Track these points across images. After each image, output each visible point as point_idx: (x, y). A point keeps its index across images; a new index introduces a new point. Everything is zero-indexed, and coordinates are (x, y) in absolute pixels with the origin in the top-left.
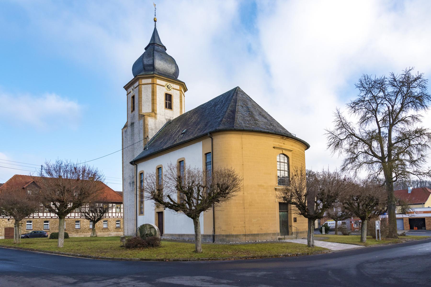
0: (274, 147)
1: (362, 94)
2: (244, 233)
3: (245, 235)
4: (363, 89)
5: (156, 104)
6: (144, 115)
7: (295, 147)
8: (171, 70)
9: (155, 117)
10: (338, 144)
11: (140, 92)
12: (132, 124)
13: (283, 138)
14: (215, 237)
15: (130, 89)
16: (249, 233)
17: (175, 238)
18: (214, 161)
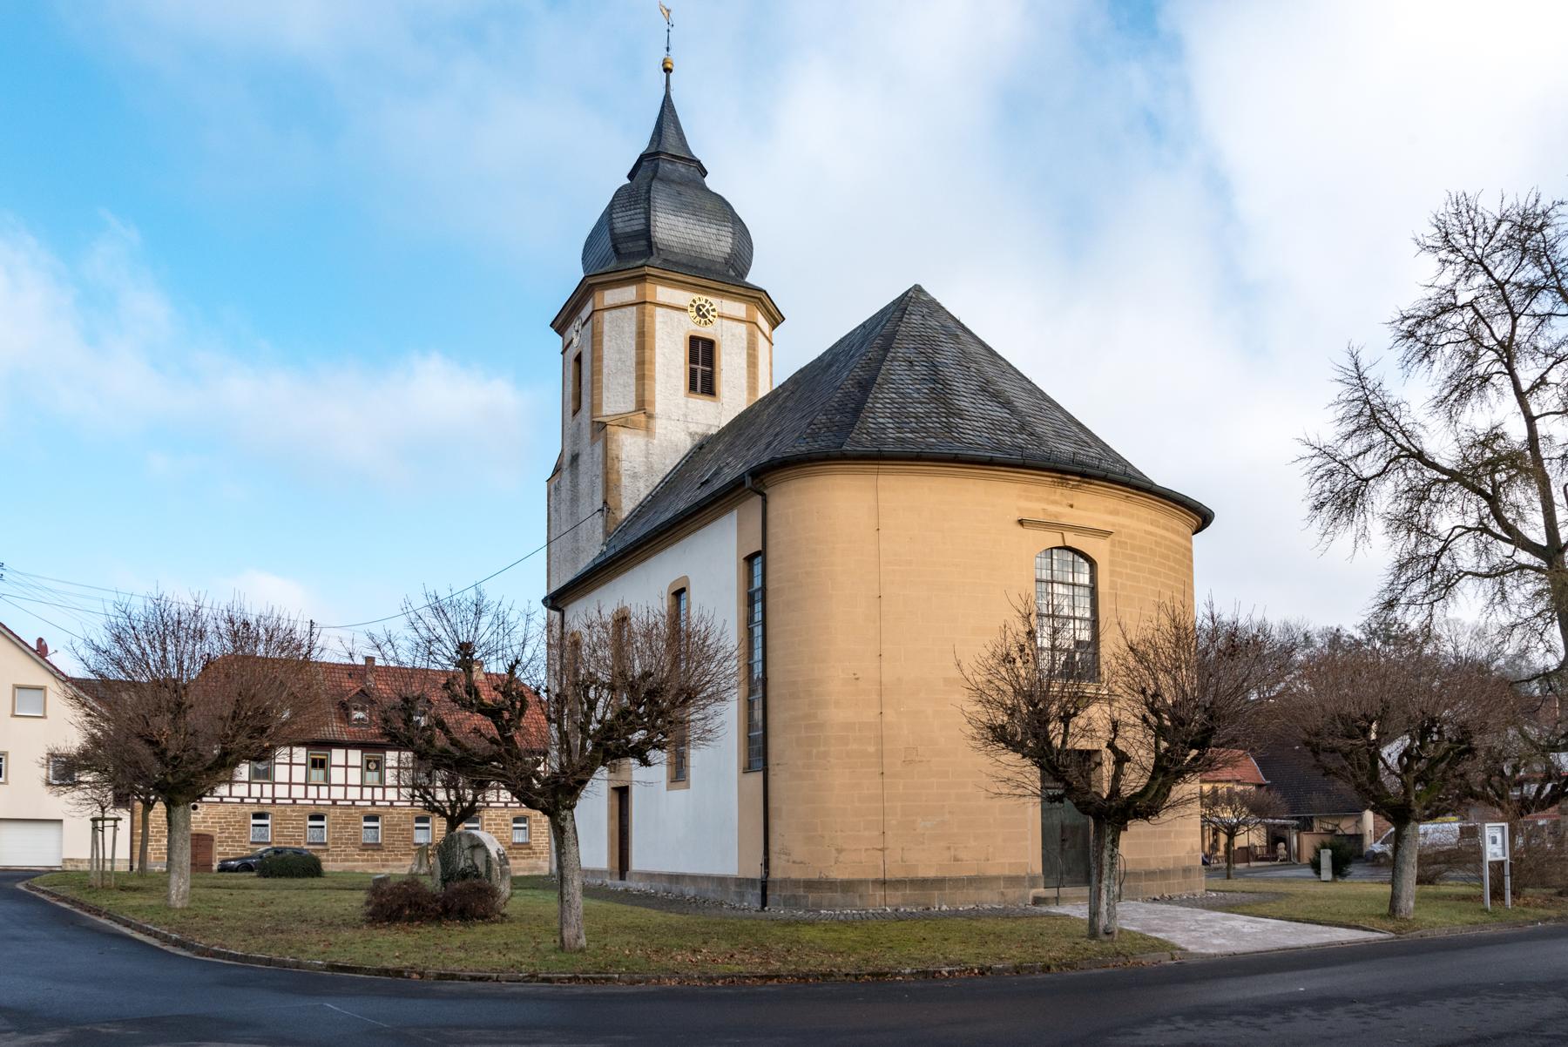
0: (1021, 522)
1: (1447, 279)
2: (881, 876)
3: (884, 883)
4: (1452, 257)
5: (653, 378)
6: (605, 425)
7: (1132, 516)
8: (717, 243)
9: (649, 430)
10: (1346, 500)
11: (596, 340)
12: (575, 458)
13: (1063, 483)
14: (770, 885)
15: (571, 332)
16: (900, 875)
17: (660, 887)
18: (771, 586)
